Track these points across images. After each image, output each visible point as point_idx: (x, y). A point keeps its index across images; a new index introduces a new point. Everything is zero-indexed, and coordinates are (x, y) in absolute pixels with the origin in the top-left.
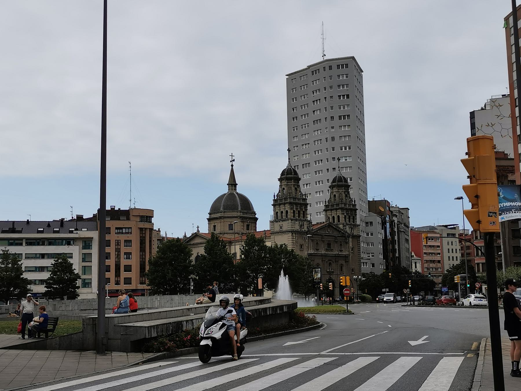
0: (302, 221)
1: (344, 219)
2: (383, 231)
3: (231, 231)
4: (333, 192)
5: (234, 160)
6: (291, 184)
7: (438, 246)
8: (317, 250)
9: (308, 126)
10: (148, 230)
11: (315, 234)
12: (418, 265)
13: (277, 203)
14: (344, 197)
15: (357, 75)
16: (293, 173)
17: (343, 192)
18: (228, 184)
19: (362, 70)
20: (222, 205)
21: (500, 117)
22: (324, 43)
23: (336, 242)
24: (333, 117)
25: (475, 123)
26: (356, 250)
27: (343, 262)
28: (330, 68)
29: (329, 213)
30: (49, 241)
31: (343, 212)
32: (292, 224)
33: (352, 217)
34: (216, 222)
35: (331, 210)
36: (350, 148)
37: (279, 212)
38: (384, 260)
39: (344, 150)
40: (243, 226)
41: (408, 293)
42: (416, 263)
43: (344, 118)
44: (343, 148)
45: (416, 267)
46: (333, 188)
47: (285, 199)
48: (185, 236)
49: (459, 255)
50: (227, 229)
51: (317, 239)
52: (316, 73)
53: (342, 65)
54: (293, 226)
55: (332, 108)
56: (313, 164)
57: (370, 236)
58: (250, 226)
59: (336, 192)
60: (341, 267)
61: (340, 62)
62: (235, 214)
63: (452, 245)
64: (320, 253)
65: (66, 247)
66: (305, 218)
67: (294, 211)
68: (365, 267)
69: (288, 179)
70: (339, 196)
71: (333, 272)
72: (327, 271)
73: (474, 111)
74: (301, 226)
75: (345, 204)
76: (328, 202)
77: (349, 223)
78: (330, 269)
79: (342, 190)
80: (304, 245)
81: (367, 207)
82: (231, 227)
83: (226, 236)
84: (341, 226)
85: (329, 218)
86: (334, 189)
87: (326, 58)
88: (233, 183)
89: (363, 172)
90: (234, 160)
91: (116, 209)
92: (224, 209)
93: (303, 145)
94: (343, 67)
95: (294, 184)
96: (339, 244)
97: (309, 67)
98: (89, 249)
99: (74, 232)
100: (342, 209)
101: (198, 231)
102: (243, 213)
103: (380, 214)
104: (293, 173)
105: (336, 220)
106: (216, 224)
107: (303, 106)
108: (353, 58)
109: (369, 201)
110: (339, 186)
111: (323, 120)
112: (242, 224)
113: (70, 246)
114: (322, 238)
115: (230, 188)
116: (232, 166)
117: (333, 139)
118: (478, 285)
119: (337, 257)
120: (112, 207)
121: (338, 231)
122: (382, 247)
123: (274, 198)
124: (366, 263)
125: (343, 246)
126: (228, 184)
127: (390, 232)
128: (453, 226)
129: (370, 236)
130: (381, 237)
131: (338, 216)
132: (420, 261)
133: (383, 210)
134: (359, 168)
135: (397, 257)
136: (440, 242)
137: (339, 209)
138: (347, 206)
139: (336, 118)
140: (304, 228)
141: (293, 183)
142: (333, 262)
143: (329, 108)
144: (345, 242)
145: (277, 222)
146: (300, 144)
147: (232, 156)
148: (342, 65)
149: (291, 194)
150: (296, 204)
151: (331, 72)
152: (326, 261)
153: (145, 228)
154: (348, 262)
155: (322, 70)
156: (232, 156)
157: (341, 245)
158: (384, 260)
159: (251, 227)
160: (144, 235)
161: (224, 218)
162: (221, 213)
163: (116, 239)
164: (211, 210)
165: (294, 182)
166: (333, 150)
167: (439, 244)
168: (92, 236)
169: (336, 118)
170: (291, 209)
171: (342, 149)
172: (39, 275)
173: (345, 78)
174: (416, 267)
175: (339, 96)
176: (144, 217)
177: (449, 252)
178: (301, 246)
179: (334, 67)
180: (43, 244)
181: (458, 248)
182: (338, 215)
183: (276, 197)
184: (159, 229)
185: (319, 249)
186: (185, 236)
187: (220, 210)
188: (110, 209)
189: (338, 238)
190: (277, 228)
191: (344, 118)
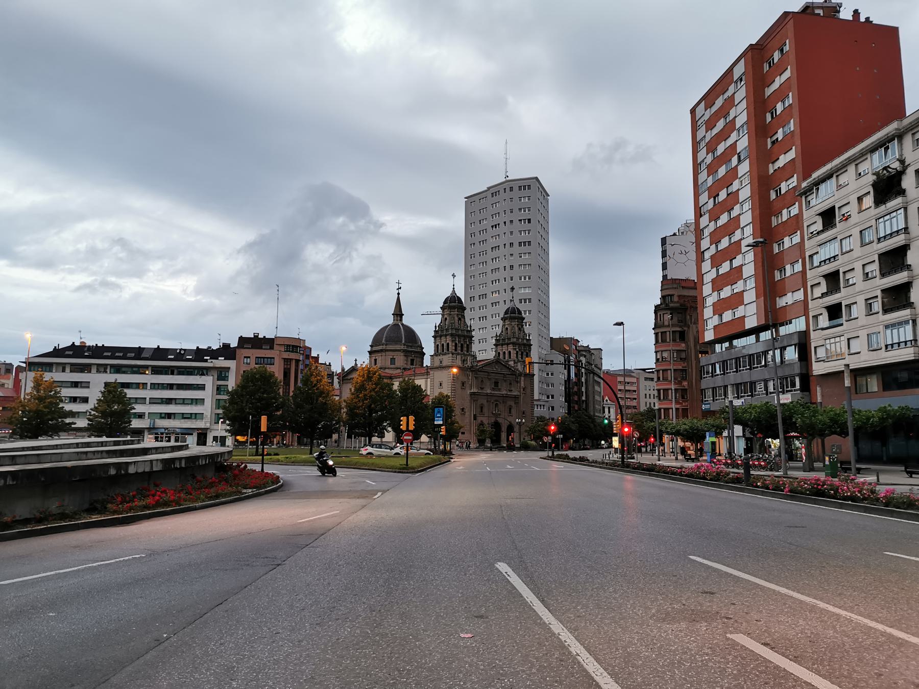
0: (465, 355)
1: (515, 355)
2: (566, 372)
3: (392, 366)
4: (505, 325)
5: (400, 288)
6: (454, 313)
7: (635, 391)
8: (482, 389)
9: (486, 254)
10: (294, 361)
11: (481, 371)
12: (612, 410)
13: (438, 334)
14: (517, 331)
15: (541, 198)
16: (457, 301)
17: (516, 326)
18: (393, 314)
19: (548, 194)
20: (385, 336)
23: (505, 381)
25: (666, 250)
26: (528, 391)
27: (512, 403)
28: (511, 189)
29: (499, 348)
30: (179, 370)
31: (515, 347)
32: (453, 358)
33: (525, 353)
34: (377, 355)
35: (502, 345)
36: (529, 279)
37: (440, 345)
38: (566, 404)
39: (523, 280)
40: (407, 361)
41: (550, 441)
42: (609, 408)
43: (525, 245)
44: (523, 278)
45: (609, 412)
46: (505, 321)
47: (446, 330)
48: (343, 369)
50: (388, 364)
51: (482, 376)
52: (496, 195)
54: (454, 361)
55: (512, 233)
56: (489, 295)
57: (550, 376)
58: (415, 361)
59: (508, 324)
60: (510, 409)
61: (522, 183)
62: (398, 347)
64: (486, 392)
65: (198, 377)
66: (470, 352)
67: (456, 344)
68: (539, 409)
69: (450, 308)
70: (511, 330)
71: (500, 414)
72: (493, 413)
73: (665, 237)
74: (463, 361)
75: (518, 339)
77: (522, 360)
78: (497, 411)
79: (515, 323)
80: (467, 383)
81: (549, 345)
82: (393, 361)
83: (387, 371)
84: (511, 363)
85: (499, 353)
86: (506, 321)
87: (507, 179)
88: (398, 313)
89: (545, 305)
90: (400, 288)
91: (261, 336)
92: (386, 341)
94: (525, 189)
95: (458, 313)
96: (508, 383)
97: (489, 188)
98: (224, 380)
99: (209, 361)
100: (514, 344)
101: (356, 364)
102: (408, 346)
103: (564, 352)
104: (457, 301)
105: (507, 356)
106: (377, 358)
108: (537, 178)
109: (551, 338)
110: (511, 318)
111: (502, 247)
112: (406, 358)
113: (203, 377)
114: (488, 376)
116: (399, 294)
117: (512, 267)
118: (637, 434)
119: (505, 397)
120: (255, 335)
121: (508, 368)
122: (563, 389)
123: (436, 328)
124: (544, 406)
125: (513, 386)
126: (393, 314)
127: (575, 373)
128: (651, 370)
129: (550, 376)
130: (563, 377)
131: (510, 352)
132: (614, 406)
133: (568, 349)
134: (539, 300)
135: (583, 401)
136: (637, 386)
137: (510, 344)
138: (520, 340)
139: (516, 245)
140: (467, 363)
141: (456, 313)
142: (500, 403)
144: (516, 381)
145: (437, 355)
146: (477, 274)
149: (453, 325)
150: (459, 336)
151: (512, 194)
152: (492, 401)
153: (291, 359)
154: (518, 403)
157: (510, 384)
158: (566, 404)
159: (416, 361)
160: (289, 367)
161: (386, 351)
162: (383, 345)
163: (842, 438)
164: (373, 342)
165: (457, 311)
166: (512, 280)
167: (635, 388)
168: (229, 366)
169: (516, 245)
170: (453, 341)
171: (521, 279)
172: (166, 407)
173: (527, 201)
174: (609, 412)
175: (519, 220)
176: (290, 347)
177: (646, 398)
178: (463, 384)
179: (516, 189)
180: (172, 373)
182: (509, 350)
183: (437, 328)
184: (330, 363)
185: (483, 388)
186: (343, 369)
187: (382, 342)
188: (253, 337)
189: (507, 376)
190: (437, 364)
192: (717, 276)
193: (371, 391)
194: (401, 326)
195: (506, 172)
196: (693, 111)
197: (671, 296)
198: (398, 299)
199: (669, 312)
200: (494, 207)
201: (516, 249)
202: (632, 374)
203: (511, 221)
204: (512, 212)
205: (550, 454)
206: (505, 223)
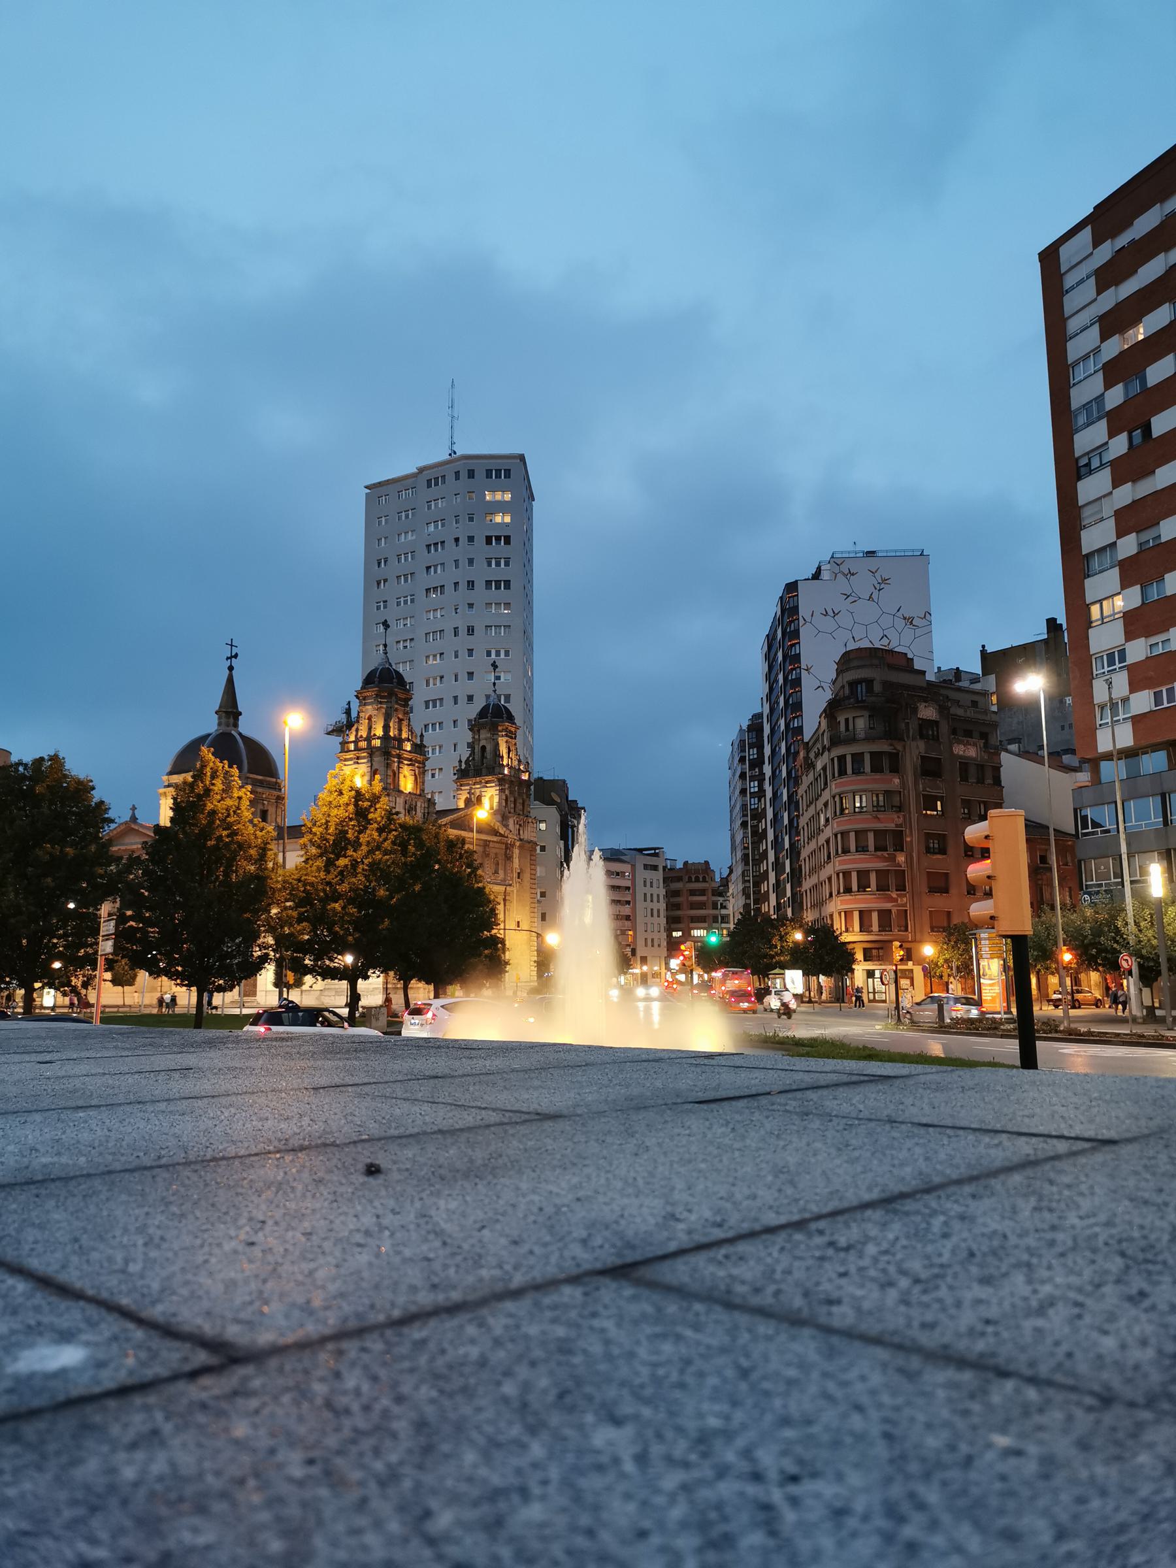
7: (628, 888)
9: (412, 601)
21: (851, 599)
22: (455, 427)
24: (473, 582)
43: (498, 587)
46: (479, 731)
49: (662, 906)
53: (498, 472)
63: (652, 886)
73: (797, 581)
76: (466, 763)
86: (481, 731)
90: (236, 656)
93: (398, 642)
97: (421, 470)
101: (134, 819)
107: (433, 503)
111: (449, 588)
115: (223, 720)
116: (231, 668)
117: (471, 631)
139: (480, 585)
143: (464, 563)
147: (232, 645)
148: (498, 472)
155: (450, 477)
156: (232, 645)
166: (470, 655)
167: (629, 884)
169: (480, 585)
181: (662, 892)
191: (498, 587)
192: (1143, 603)
193: (371, 852)
194: (238, 737)
195: (453, 443)
196: (1049, 258)
197: (869, 682)
198: (230, 682)
199: (866, 714)
200: (403, 518)
201: (480, 594)
202: (622, 857)
203: (471, 539)
204: (471, 519)
205: (186, 997)
206: (457, 540)
